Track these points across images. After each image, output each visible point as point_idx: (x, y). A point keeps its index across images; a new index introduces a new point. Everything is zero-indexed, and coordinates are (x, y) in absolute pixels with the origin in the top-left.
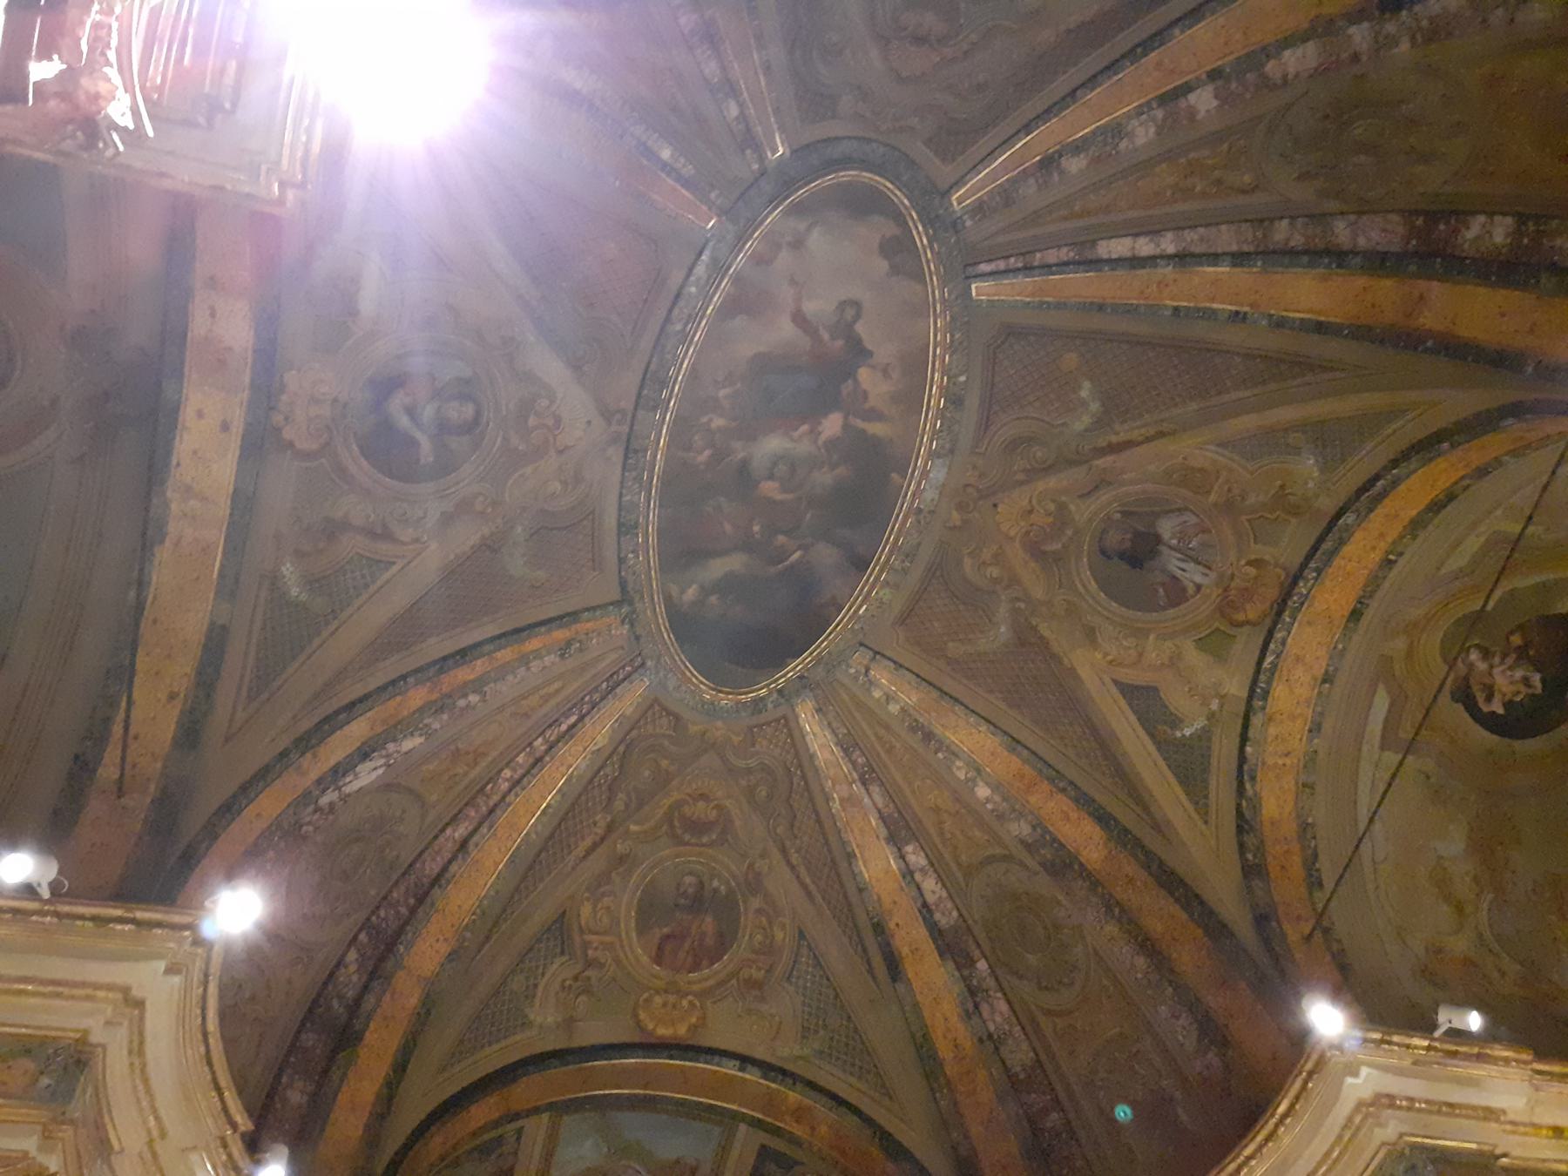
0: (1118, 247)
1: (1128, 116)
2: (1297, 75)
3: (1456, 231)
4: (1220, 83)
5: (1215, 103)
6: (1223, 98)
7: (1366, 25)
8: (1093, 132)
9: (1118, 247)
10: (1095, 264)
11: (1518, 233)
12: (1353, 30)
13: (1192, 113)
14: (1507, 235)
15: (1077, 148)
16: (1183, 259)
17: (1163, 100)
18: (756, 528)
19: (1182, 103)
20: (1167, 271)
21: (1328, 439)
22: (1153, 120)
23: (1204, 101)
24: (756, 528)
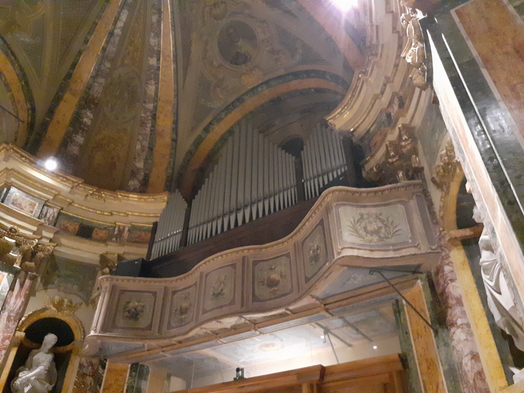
0: (124, 17)
1: (159, 41)
2: (147, 87)
3: (90, 109)
4: (155, 68)
5: (150, 64)
6: (151, 67)
7: (152, 108)
8: (160, 29)
9: (124, 17)
10: (122, 7)
11: (85, 124)
12: (152, 105)
13: (152, 57)
14: (85, 122)
15: (159, 22)
16: (111, 34)
17: (159, 52)
18: (341, 179)
19: (155, 55)
20: (110, 27)
21: (36, 52)
22: (155, 46)
23: (153, 61)
24: (341, 179)
